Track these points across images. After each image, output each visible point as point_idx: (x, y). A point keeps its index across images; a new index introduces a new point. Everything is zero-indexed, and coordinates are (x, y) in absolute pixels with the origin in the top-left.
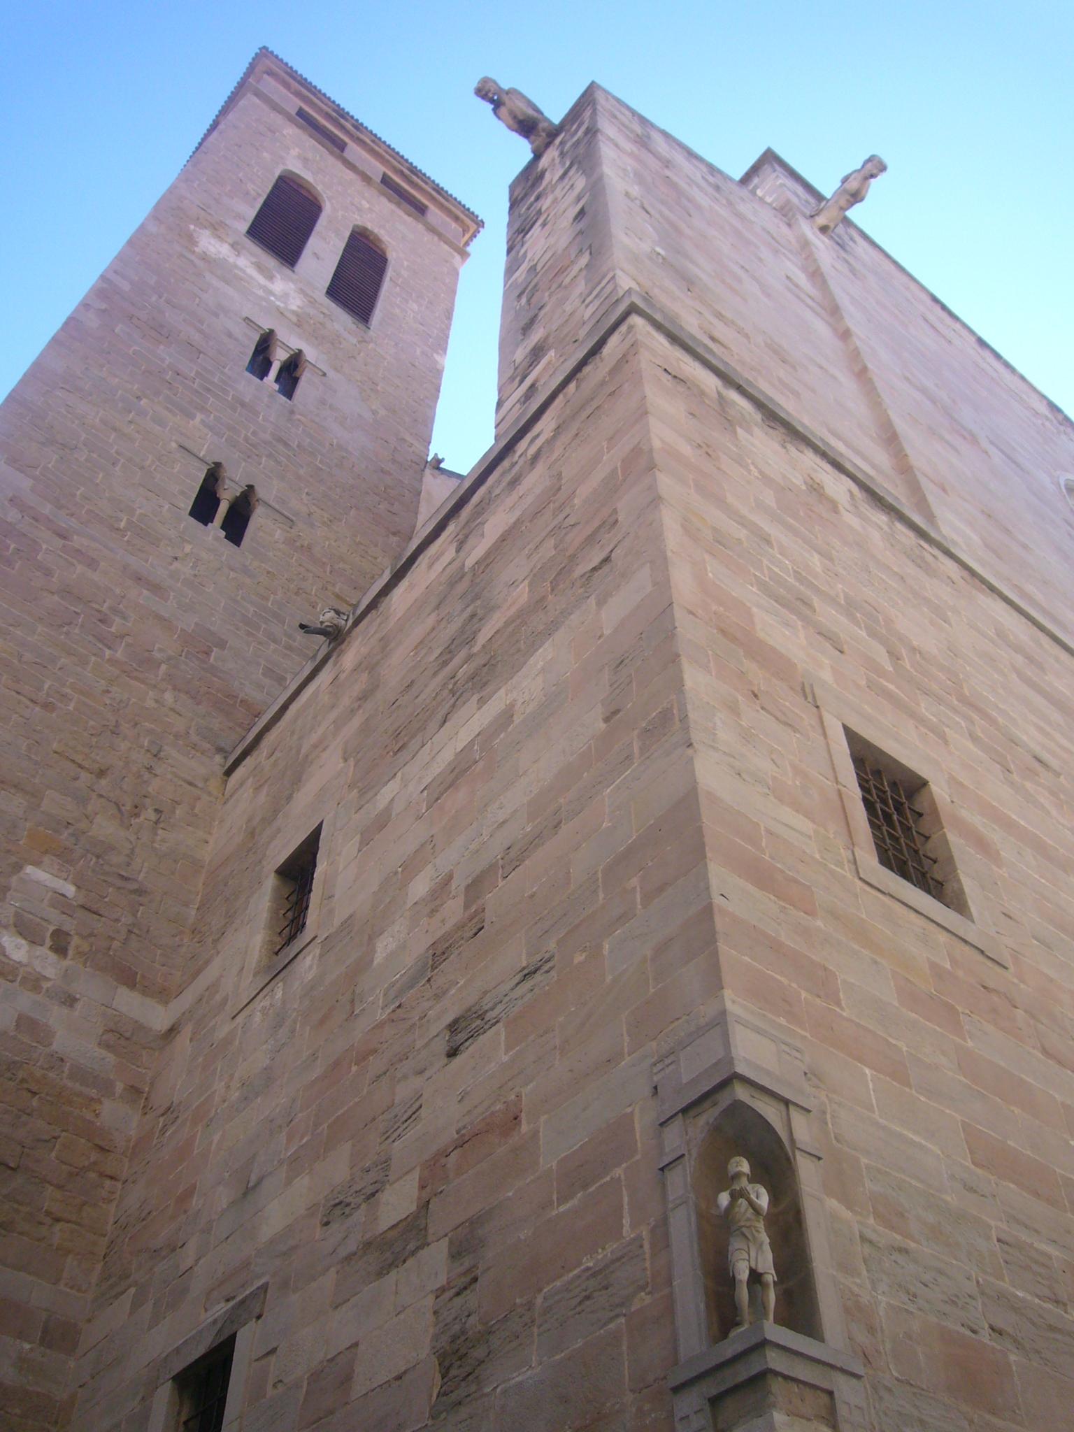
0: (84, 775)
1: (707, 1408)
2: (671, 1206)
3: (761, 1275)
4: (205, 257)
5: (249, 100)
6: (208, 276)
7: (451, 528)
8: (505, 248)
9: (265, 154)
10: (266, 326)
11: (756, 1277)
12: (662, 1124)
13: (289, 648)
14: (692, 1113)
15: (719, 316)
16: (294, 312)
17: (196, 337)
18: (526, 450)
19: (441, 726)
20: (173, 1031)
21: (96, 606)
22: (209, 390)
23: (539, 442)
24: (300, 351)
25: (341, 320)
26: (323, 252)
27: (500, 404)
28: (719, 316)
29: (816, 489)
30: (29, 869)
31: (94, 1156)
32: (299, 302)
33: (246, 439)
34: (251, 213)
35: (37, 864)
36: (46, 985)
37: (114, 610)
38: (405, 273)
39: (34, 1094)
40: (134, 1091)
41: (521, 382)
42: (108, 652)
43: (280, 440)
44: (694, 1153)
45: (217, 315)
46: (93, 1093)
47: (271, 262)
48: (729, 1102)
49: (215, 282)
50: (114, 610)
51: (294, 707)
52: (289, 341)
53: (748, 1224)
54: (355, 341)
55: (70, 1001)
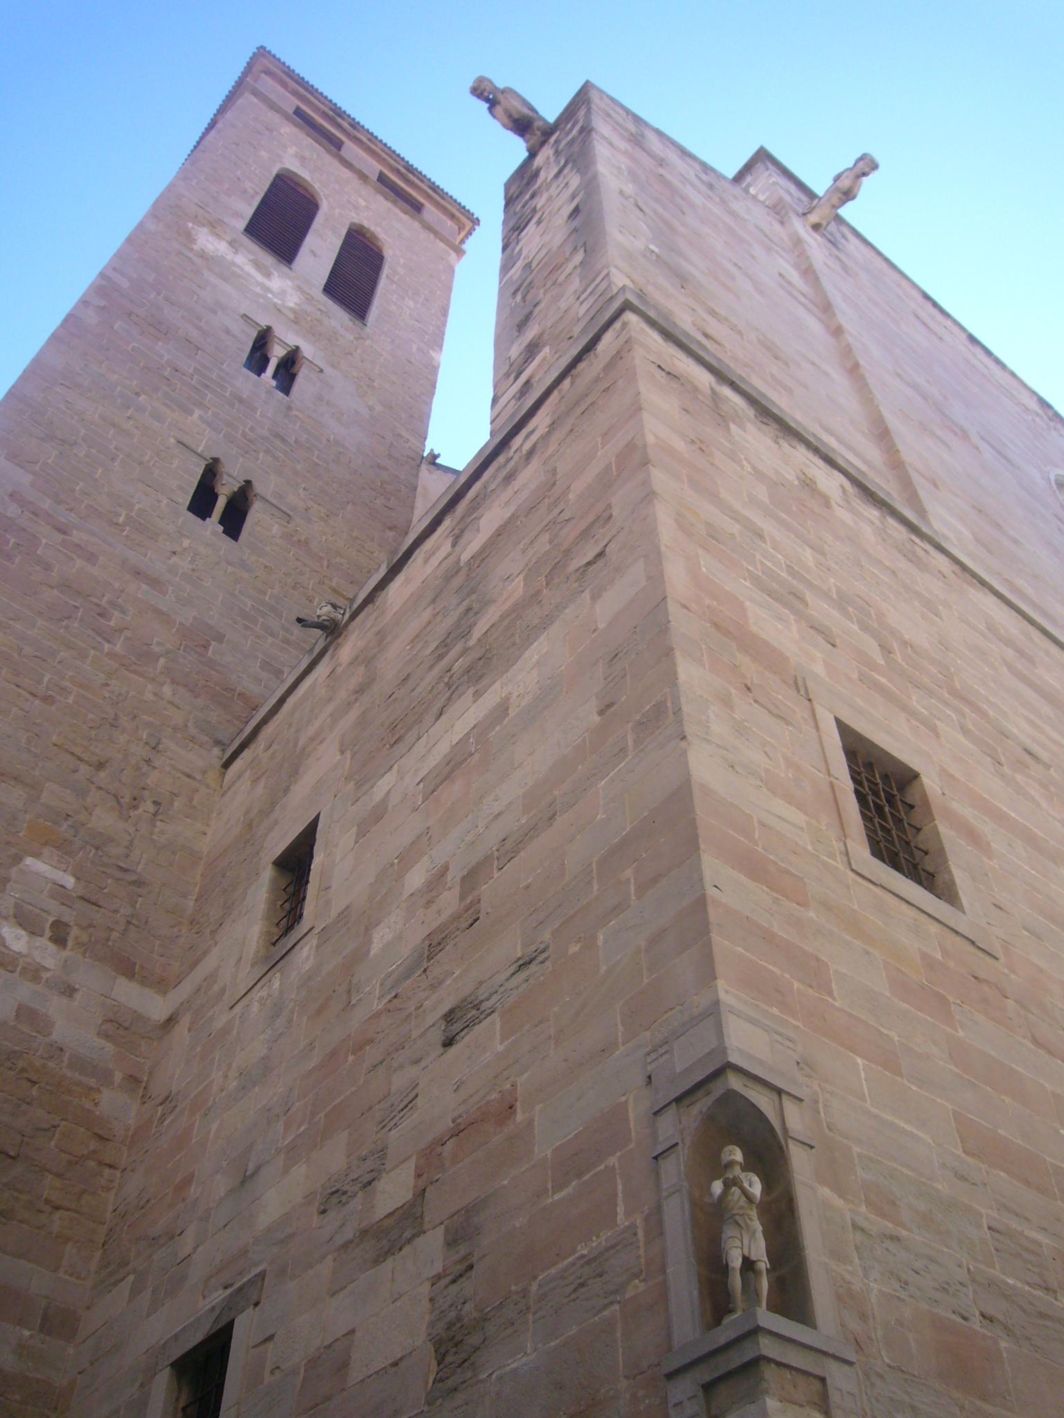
0: (83, 768)
1: (701, 1394)
2: (664, 1194)
3: (754, 1262)
4: (203, 255)
5: (247, 99)
6: (206, 273)
7: (447, 523)
8: (500, 245)
9: (263, 153)
10: (264, 323)
11: (749, 1265)
12: (655, 1114)
13: (286, 641)
14: (686, 1102)
15: (713, 313)
16: (291, 309)
17: (194, 334)
18: (521, 446)
19: (437, 719)
20: (171, 1021)
21: (95, 600)
22: (207, 386)
23: (534, 438)
24: (297, 348)
25: (338, 317)
26: (320, 250)
27: (495, 401)
28: (713, 313)
29: (808, 484)
30: (29, 861)
31: (93, 1145)
32: (296, 299)
33: (244, 435)
34: (249, 211)
35: (37, 855)
36: (45, 975)
37: (113, 604)
38: (401, 271)
39: (34, 1083)
40: (133, 1080)
41: (517, 378)
42: (107, 646)
43: (277, 436)
44: (688, 1141)
45: (215, 312)
46: (92, 1082)
47: (268, 259)
48: (722, 1091)
49: (213, 279)
50: (113, 604)
51: (291, 701)
52: (286, 338)
53: (741, 1212)
54: (351, 338)
55: (70, 991)
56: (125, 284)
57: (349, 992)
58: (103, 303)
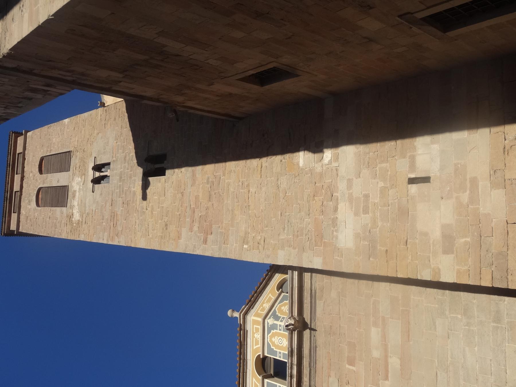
4: (82, 216)
6: (87, 212)
8: (8, 121)
10: (91, 185)
16: (81, 179)
17: (109, 204)
18: (69, 76)
19: (180, 55)
21: (210, 189)
22: (123, 191)
23: (64, 73)
24: (93, 169)
25: (75, 161)
26: (55, 179)
27: (61, 94)
32: (77, 179)
33: (131, 171)
34: (58, 210)
37: (208, 182)
38: (45, 149)
41: (48, 91)
43: (125, 159)
45: (98, 202)
49: (87, 209)
51: (206, 109)
52: (91, 174)
54: (78, 153)
56: (106, 234)
57: (289, 38)
58: (116, 237)
